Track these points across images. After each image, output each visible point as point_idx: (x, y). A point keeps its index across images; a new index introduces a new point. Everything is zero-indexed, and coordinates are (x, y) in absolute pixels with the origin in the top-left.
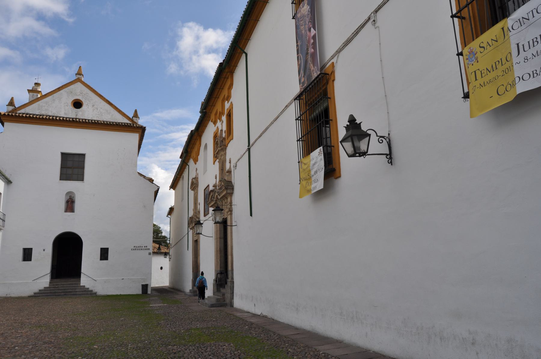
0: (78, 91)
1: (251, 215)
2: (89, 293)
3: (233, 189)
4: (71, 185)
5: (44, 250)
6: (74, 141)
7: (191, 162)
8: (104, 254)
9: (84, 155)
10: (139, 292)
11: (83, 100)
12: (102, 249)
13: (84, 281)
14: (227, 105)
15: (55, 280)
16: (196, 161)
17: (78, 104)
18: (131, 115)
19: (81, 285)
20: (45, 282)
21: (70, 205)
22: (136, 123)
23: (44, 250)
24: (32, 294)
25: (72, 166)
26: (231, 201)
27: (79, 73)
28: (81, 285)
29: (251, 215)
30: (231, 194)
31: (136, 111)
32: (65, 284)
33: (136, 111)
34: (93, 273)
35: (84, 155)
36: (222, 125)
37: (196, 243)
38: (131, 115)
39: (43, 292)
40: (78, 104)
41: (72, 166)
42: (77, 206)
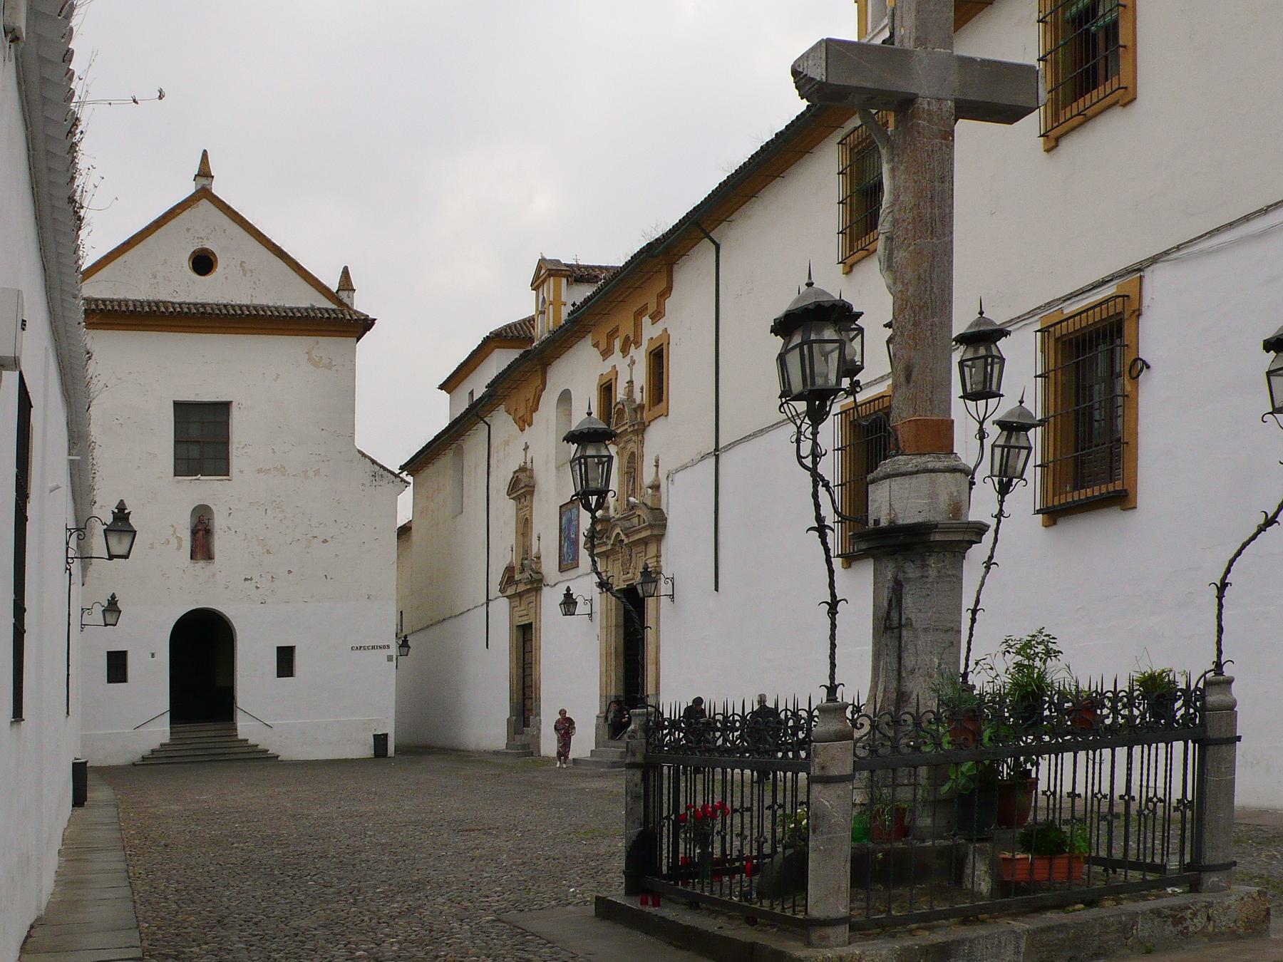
0: (204, 229)
1: (717, 590)
2: (259, 758)
3: (665, 526)
4: (203, 489)
5: (153, 656)
6: (204, 366)
7: (502, 421)
8: (285, 661)
9: (225, 407)
10: (367, 751)
11: (208, 246)
12: (111, 655)
13: (246, 728)
14: (650, 331)
15: (181, 727)
16: (524, 422)
17: (203, 263)
18: (333, 284)
19: (240, 737)
20: (160, 732)
21: (202, 540)
22: (349, 308)
23: (153, 656)
24: (137, 758)
25: (202, 436)
26: (659, 551)
27: (204, 173)
28: (240, 737)
29: (717, 590)
30: (659, 538)
31: (346, 272)
32: (205, 732)
33: (346, 272)
34: (264, 708)
35: (225, 407)
36: (632, 372)
37: (525, 634)
38: (333, 284)
39: (156, 755)
40: (203, 263)
41: (202, 436)
42: (220, 543)
